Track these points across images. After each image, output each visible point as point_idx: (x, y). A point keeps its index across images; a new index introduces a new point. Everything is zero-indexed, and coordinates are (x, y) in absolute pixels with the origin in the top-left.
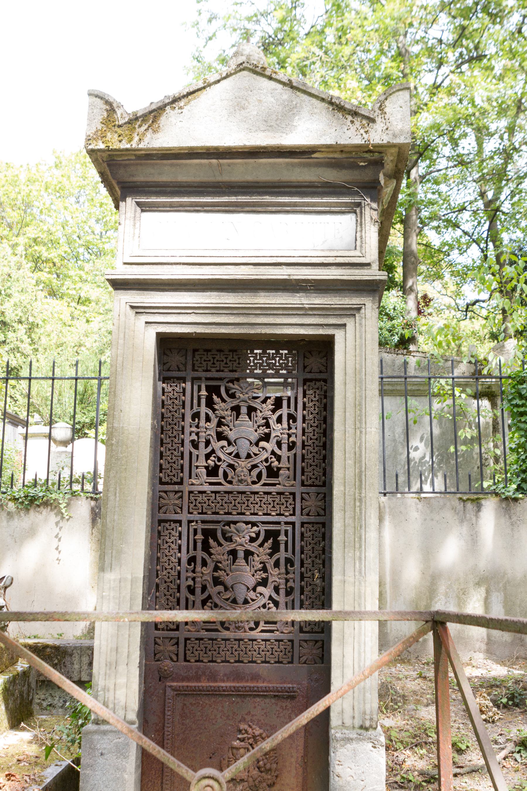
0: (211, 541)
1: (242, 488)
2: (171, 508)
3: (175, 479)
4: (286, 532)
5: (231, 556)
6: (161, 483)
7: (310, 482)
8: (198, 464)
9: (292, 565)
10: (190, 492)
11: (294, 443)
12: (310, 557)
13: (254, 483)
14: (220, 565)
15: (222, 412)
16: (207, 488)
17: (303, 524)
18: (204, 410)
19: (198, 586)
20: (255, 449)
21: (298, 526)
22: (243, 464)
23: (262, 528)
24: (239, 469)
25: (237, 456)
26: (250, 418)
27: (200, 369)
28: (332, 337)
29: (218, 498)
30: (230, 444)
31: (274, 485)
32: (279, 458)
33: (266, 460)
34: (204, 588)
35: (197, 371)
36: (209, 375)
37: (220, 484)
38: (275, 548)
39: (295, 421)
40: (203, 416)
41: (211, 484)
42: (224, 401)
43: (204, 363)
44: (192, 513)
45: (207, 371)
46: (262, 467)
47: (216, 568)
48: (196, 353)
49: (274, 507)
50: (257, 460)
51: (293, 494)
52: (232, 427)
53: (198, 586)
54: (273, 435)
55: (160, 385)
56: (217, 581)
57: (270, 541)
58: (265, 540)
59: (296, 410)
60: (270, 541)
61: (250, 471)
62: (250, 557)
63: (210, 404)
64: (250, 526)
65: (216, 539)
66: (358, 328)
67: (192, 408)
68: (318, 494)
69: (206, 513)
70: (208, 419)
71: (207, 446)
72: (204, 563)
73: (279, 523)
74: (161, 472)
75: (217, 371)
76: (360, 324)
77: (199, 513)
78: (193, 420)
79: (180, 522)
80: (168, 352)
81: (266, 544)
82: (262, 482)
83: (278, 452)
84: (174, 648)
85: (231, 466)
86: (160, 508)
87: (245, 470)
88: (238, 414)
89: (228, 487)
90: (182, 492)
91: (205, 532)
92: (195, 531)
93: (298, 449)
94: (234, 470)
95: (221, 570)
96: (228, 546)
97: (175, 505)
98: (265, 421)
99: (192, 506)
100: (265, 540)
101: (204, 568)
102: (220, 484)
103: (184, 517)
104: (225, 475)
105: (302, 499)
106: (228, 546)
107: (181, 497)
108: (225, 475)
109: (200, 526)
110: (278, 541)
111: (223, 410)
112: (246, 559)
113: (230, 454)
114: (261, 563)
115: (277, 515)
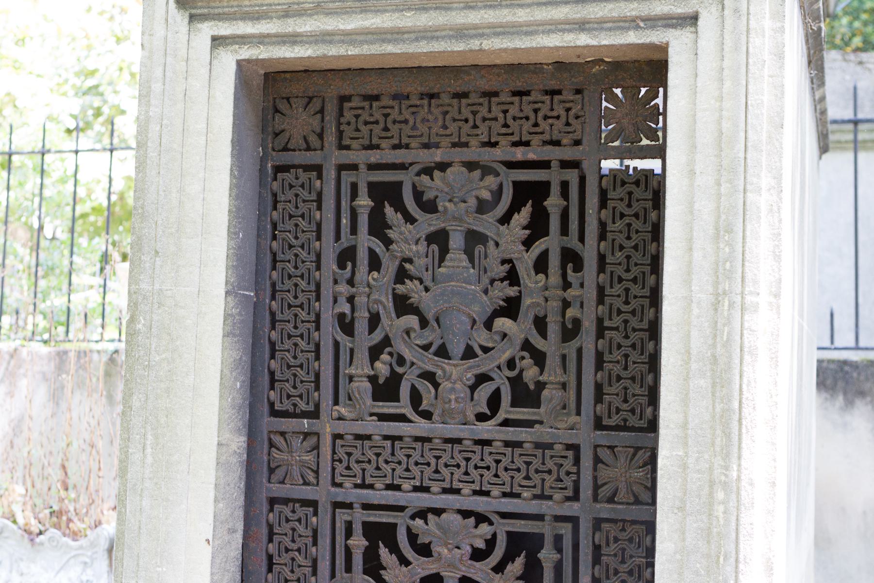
0: (389, 210)
1: (453, 430)
2: (296, 471)
3: (303, 406)
4: (558, 539)
5: (435, 247)
6: (275, 413)
7: (614, 420)
8: (352, 371)
9: (578, 268)
10: (337, 437)
11: (577, 323)
12: (616, 540)
13: (481, 417)
14: (407, 266)
15: (404, 247)
16: (371, 426)
17: (597, 524)
18: (365, 241)
19: (362, 316)
20: (482, 337)
21: (585, 528)
22: (455, 373)
23: (502, 528)
24: (445, 385)
25: (443, 352)
26: (471, 260)
27: (355, 144)
28: (664, 49)
29: (398, 452)
30: (424, 323)
31: (529, 424)
32: (539, 358)
33: (511, 364)
34: (374, 321)
35: (348, 148)
36: (374, 157)
37: (402, 418)
38: (538, 227)
39: (579, 267)
40: (362, 256)
41: (383, 417)
42: (410, 219)
43: (365, 129)
44: (340, 485)
45: (371, 147)
46: (501, 382)
47: (402, 276)
48: (347, 105)
49: (527, 478)
50: (484, 364)
51: (575, 448)
52: (429, 283)
53: (362, 316)
54: (526, 302)
55: (267, 422)
56: (403, 306)
57: (520, 561)
58: (508, 558)
59: (582, 239)
60: (520, 561)
61: (473, 388)
62: (479, 249)
63: (379, 227)
64: (472, 520)
65: (400, 207)
66: (729, 22)
67: (338, 238)
68: (637, 449)
69: (371, 487)
70: (375, 264)
71: (372, 330)
72: (375, 264)
73: (540, 517)
74: (273, 298)
75: (395, 147)
76: (736, 11)
77: (356, 486)
78: (342, 266)
79: (313, 504)
80: (282, 106)
81: (509, 567)
82: (501, 415)
83: (538, 342)
84: (309, 458)
85: (429, 376)
86: (271, 471)
87: (458, 386)
88: (444, 251)
89: (421, 427)
90: (318, 434)
91: (373, 531)
92: (354, 187)
93: (587, 340)
94: (436, 385)
95: (411, 278)
96: (428, 223)
97: (303, 464)
98: (507, 267)
99: (340, 468)
100: (508, 558)
101: (375, 274)
102: (402, 418)
103: (323, 493)
104: (416, 398)
105: (597, 460)
106: (428, 223)
107: (317, 447)
108: (416, 398)
109: (359, 516)
110: (545, 208)
111: (406, 241)
112: (469, 252)
113: (426, 348)
114: (504, 262)
115: (536, 497)
